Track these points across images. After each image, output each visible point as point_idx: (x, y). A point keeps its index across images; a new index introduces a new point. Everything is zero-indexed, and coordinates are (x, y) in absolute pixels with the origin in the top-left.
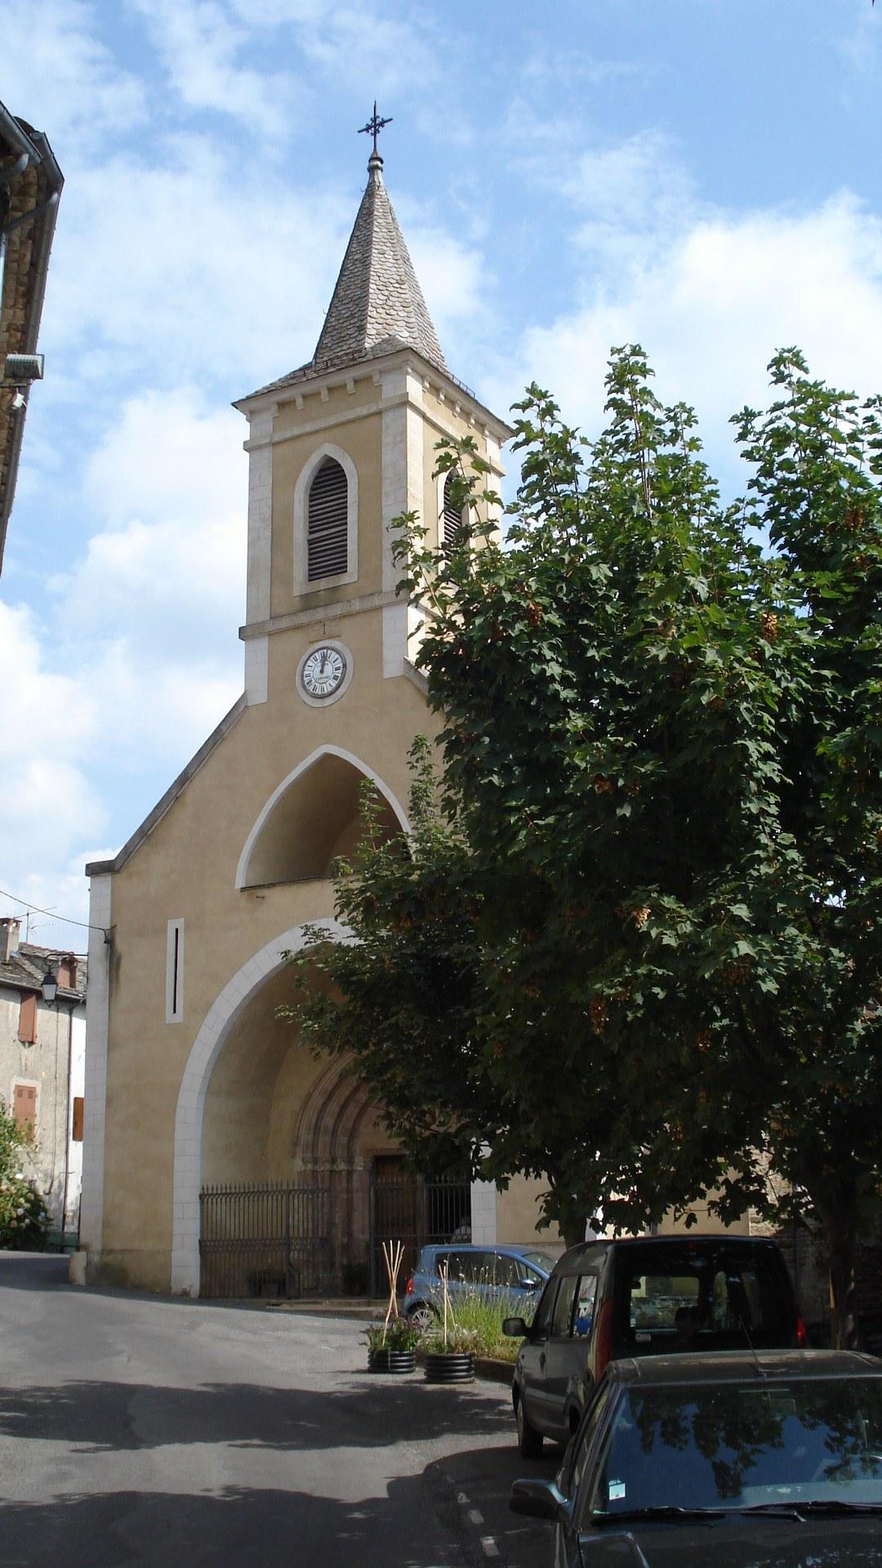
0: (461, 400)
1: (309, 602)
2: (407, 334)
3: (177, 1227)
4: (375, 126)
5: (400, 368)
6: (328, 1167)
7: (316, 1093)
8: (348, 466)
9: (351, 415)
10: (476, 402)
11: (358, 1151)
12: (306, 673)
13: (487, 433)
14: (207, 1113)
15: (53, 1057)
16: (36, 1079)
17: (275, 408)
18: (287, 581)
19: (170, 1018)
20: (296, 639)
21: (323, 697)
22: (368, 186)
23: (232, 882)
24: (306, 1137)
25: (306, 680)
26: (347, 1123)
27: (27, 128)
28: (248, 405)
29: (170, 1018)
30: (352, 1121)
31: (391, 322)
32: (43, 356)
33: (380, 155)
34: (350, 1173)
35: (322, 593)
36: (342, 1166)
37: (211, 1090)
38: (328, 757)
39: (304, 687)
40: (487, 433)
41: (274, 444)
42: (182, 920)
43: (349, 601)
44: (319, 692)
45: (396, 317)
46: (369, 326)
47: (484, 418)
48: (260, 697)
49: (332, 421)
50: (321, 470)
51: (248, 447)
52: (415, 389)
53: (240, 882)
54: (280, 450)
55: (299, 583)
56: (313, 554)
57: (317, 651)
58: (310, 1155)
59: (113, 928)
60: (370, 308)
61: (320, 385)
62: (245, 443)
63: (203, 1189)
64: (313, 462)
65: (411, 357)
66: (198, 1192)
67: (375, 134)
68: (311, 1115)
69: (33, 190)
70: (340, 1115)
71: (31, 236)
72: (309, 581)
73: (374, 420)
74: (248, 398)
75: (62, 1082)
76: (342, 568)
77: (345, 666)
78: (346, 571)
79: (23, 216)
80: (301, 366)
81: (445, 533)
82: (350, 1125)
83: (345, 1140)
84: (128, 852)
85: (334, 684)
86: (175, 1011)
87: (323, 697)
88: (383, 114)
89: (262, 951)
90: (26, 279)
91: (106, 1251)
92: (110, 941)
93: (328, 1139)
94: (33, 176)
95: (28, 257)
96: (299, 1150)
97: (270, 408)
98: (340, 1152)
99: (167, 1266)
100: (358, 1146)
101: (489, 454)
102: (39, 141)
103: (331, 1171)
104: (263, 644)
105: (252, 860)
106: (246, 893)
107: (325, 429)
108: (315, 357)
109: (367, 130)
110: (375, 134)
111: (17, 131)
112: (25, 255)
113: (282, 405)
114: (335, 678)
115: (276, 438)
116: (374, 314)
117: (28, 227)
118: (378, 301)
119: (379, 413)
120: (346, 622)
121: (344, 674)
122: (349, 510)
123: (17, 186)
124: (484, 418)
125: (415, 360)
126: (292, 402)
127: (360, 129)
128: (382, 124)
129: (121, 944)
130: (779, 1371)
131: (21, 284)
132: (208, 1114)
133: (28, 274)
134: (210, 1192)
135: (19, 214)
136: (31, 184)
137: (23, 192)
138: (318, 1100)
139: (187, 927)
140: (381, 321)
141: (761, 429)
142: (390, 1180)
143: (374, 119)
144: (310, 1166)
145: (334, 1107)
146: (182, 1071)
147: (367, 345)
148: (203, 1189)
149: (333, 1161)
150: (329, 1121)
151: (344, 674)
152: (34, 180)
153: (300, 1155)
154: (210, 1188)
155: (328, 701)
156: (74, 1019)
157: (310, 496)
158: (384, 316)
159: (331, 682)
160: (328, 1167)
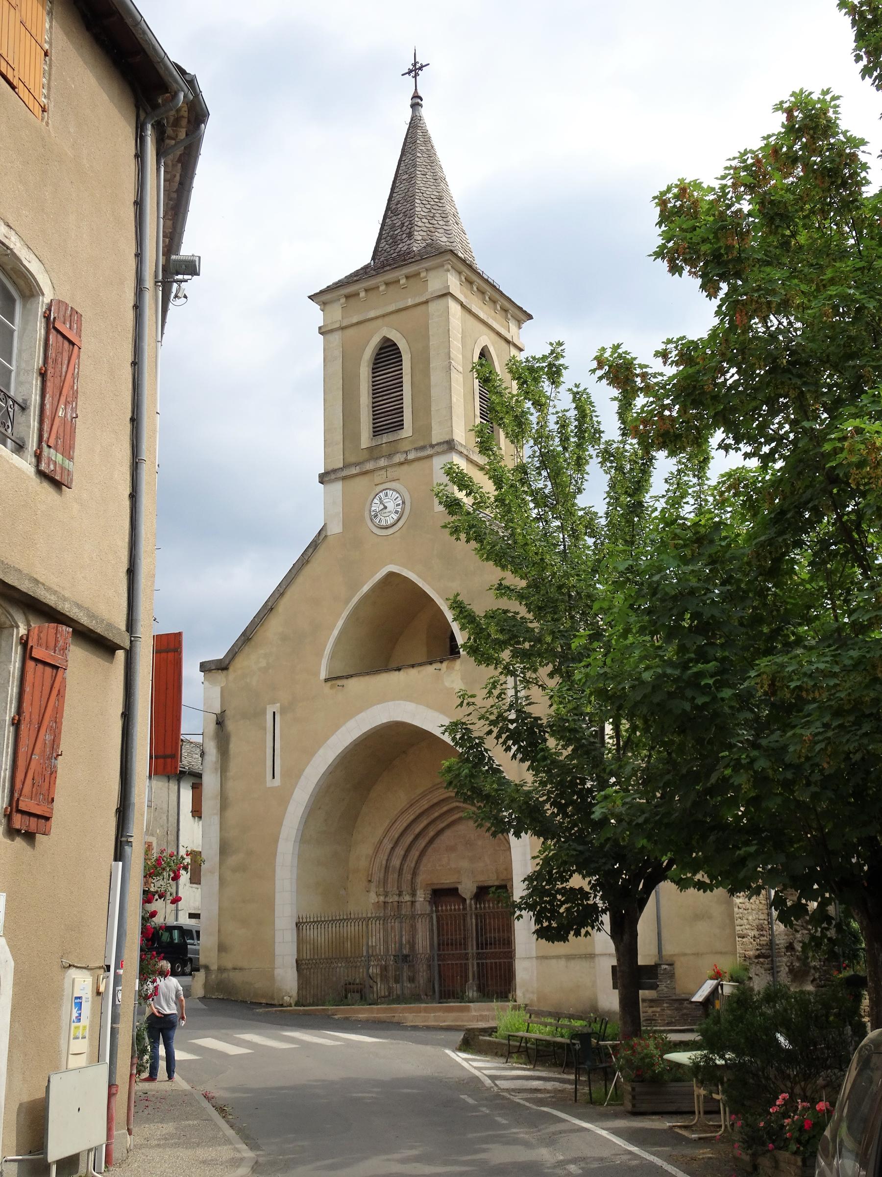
0: (489, 291)
1: (373, 453)
2: (446, 239)
3: (279, 949)
4: (415, 70)
5: (443, 266)
6: (396, 898)
7: (385, 841)
8: (402, 345)
9: (401, 305)
10: (501, 292)
11: (419, 886)
12: (373, 508)
13: (509, 316)
14: (300, 856)
15: (165, 818)
16: (152, 835)
17: (343, 300)
18: (357, 437)
19: (270, 783)
20: (361, 483)
21: (386, 528)
22: (412, 120)
23: (318, 674)
24: (378, 875)
26: (411, 863)
27: (183, 72)
28: (321, 298)
29: (270, 783)
30: (414, 862)
31: (433, 230)
32: (200, 258)
33: (420, 93)
34: (413, 903)
36: (407, 898)
37: (304, 839)
38: (391, 574)
40: (509, 316)
41: (343, 328)
42: (278, 705)
44: (383, 523)
45: (437, 226)
46: (416, 233)
47: (507, 305)
48: (335, 528)
49: (392, 308)
50: (381, 349)
51: (322, 331)
52: (454, 283)
53: (323, 675)
54: (350, 332)
55: (365, 439)
56: (376, 416)
57: (381, 492)
58: (382, 889)
59: (223, 712)
60: (417, 219)
61: (379, 280)
62: (320, 328)
64: (375, 342)
65: (449, 256)
66: (295, 920)
68: (382, 858)
69: (184, 122)
70: (405, 857)
71: (179, 160)
73: (423, 307)
74: (322, 292)
75: (172, 838)
76: (400, 426)
77: (404, 503)
79: (175, 144)
80: (362, 266)
82: (413, 865)
83: (409, 877)
84: (234, 653)
85: (395, 517)
86: (274, 777)
87: (386, 528)
88: (421, 60)
89: (343, 729)
90: (175, 195)
91: (221, 970)
92: (220, 722)
93: (396, 876)
94: (184, 113)
95: (178, 178)
96: (373, 885)
97: (339, 300)
98: (405, 887)
99: (271, 977)
100: (421, 879)
101: (511, 334)
102: (191, 82)
103: (385, 903)
104: (337, 487)
105: (333, 656)
106: (329, 684)
107: (384, 316)
108: (373, 258)
109: (409, 73)
110: (415, 77)
111: (175, 73)
112: (175, 176)
113: (347, 297)
114: (396, 512)
115: (344, 325)
116: (420, 224)
117: (178, 153)
118: (422, 213)
119: (426, 302)
120: (405, 468)
121: (403, 509)
122: (404, 379)
123: (172, 119)
124: (507, 305)
125: (454, 260)
126: (357, 294)
128: (421, 68)
129: (230, 726)
131: (170, 200)
132: (302, 859)
133: (177, 191)
134: (305, 920)
135: (173, 142)
136: (183, 117)
137: (176, 123)
138: (387, 845)
139: (283, 711)
140: (425, 229)
142: (449, 908)
143: (415, 65)
144: (382, 898)
145: (400, 851)
146: (280, 824)
147: (415, 249)
149: (400, 894)
150: (396, 862)
151: (403, 509)
152: (186, 114)
153: (373, 888)
155: (390, 531)
156: (182, 790)
157: (373, 369)
158: (427, 225)
159: (393, 515)
160: (396, 898)
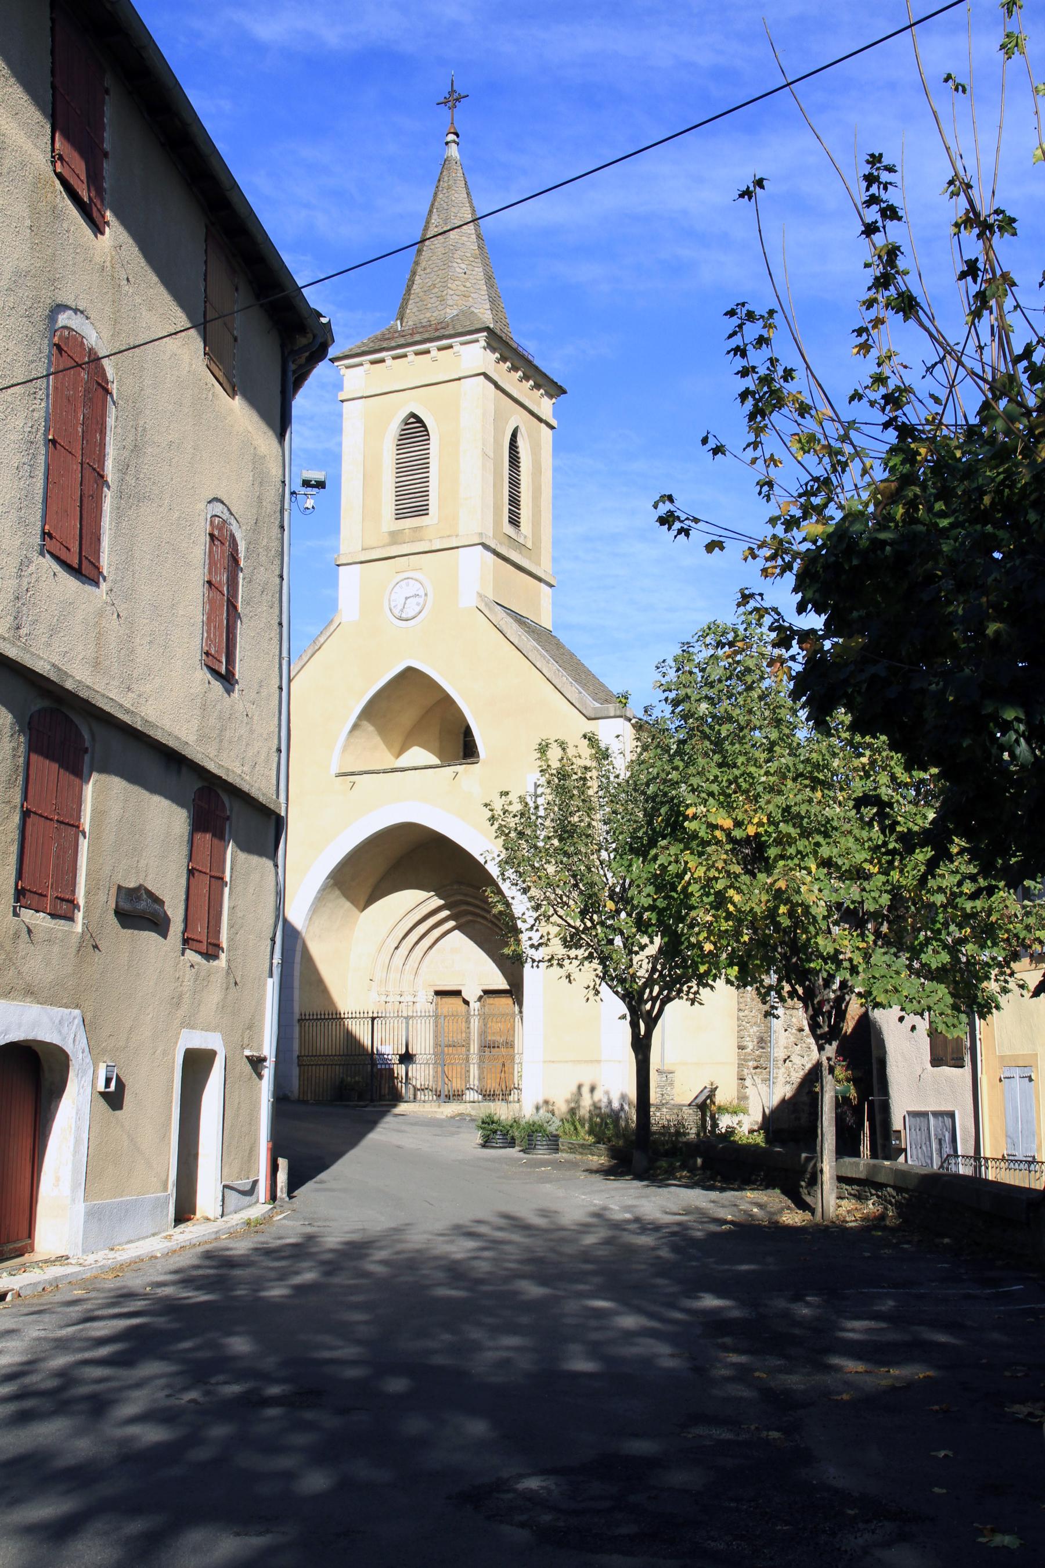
25: (393, 604)
35: (407, 531)
39: (389, 600)
43: (430, 541)
53: (335, 769)
63: (326, 1220)
67: (453, 91)
72: (397, 519)
78: (427, 514)
81: (510, 482)
127: (439, 101)
130: (708, 1119)
141: (622, 744)
148: (326, 1220)
154: (307, 1014)
